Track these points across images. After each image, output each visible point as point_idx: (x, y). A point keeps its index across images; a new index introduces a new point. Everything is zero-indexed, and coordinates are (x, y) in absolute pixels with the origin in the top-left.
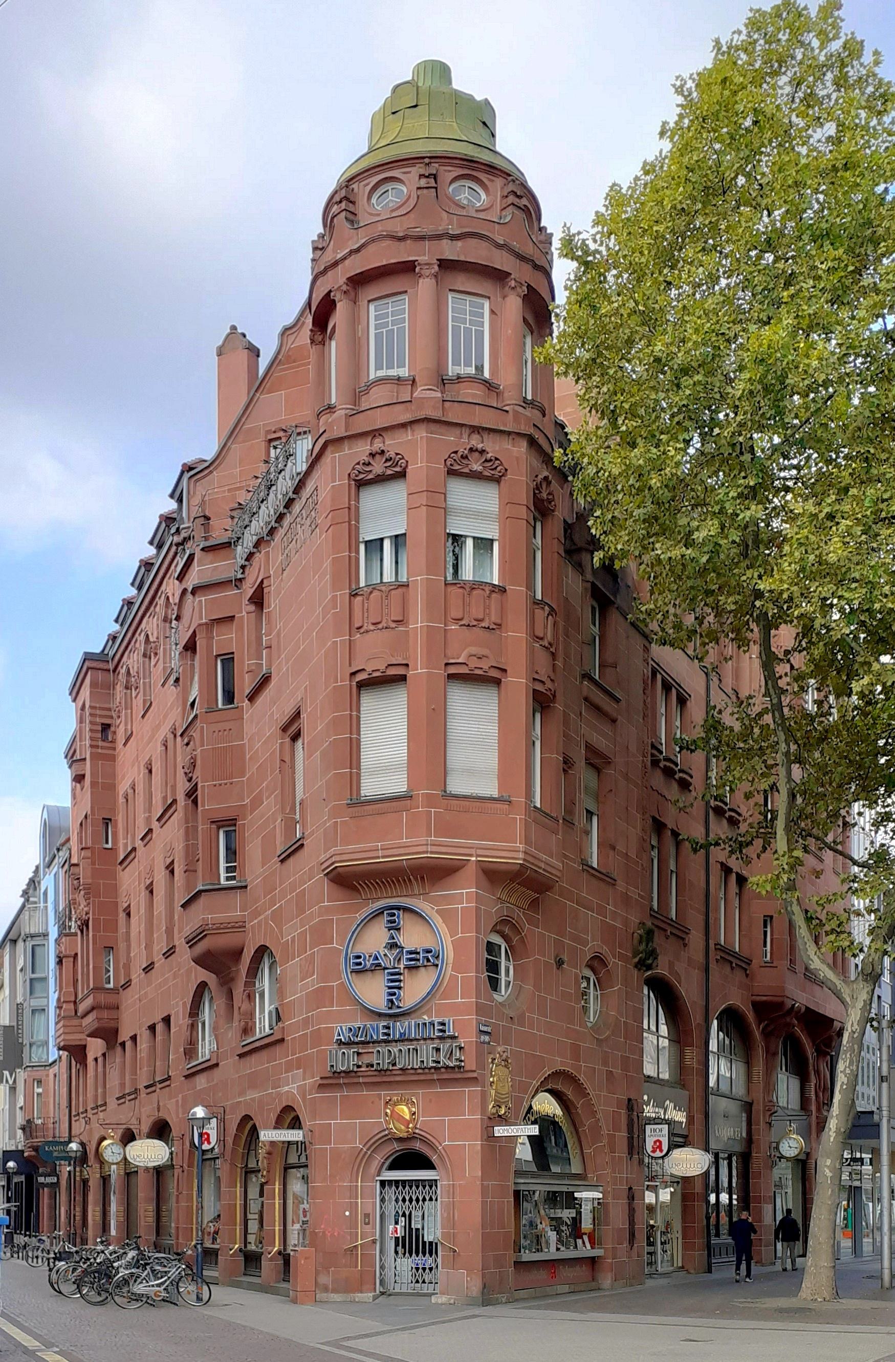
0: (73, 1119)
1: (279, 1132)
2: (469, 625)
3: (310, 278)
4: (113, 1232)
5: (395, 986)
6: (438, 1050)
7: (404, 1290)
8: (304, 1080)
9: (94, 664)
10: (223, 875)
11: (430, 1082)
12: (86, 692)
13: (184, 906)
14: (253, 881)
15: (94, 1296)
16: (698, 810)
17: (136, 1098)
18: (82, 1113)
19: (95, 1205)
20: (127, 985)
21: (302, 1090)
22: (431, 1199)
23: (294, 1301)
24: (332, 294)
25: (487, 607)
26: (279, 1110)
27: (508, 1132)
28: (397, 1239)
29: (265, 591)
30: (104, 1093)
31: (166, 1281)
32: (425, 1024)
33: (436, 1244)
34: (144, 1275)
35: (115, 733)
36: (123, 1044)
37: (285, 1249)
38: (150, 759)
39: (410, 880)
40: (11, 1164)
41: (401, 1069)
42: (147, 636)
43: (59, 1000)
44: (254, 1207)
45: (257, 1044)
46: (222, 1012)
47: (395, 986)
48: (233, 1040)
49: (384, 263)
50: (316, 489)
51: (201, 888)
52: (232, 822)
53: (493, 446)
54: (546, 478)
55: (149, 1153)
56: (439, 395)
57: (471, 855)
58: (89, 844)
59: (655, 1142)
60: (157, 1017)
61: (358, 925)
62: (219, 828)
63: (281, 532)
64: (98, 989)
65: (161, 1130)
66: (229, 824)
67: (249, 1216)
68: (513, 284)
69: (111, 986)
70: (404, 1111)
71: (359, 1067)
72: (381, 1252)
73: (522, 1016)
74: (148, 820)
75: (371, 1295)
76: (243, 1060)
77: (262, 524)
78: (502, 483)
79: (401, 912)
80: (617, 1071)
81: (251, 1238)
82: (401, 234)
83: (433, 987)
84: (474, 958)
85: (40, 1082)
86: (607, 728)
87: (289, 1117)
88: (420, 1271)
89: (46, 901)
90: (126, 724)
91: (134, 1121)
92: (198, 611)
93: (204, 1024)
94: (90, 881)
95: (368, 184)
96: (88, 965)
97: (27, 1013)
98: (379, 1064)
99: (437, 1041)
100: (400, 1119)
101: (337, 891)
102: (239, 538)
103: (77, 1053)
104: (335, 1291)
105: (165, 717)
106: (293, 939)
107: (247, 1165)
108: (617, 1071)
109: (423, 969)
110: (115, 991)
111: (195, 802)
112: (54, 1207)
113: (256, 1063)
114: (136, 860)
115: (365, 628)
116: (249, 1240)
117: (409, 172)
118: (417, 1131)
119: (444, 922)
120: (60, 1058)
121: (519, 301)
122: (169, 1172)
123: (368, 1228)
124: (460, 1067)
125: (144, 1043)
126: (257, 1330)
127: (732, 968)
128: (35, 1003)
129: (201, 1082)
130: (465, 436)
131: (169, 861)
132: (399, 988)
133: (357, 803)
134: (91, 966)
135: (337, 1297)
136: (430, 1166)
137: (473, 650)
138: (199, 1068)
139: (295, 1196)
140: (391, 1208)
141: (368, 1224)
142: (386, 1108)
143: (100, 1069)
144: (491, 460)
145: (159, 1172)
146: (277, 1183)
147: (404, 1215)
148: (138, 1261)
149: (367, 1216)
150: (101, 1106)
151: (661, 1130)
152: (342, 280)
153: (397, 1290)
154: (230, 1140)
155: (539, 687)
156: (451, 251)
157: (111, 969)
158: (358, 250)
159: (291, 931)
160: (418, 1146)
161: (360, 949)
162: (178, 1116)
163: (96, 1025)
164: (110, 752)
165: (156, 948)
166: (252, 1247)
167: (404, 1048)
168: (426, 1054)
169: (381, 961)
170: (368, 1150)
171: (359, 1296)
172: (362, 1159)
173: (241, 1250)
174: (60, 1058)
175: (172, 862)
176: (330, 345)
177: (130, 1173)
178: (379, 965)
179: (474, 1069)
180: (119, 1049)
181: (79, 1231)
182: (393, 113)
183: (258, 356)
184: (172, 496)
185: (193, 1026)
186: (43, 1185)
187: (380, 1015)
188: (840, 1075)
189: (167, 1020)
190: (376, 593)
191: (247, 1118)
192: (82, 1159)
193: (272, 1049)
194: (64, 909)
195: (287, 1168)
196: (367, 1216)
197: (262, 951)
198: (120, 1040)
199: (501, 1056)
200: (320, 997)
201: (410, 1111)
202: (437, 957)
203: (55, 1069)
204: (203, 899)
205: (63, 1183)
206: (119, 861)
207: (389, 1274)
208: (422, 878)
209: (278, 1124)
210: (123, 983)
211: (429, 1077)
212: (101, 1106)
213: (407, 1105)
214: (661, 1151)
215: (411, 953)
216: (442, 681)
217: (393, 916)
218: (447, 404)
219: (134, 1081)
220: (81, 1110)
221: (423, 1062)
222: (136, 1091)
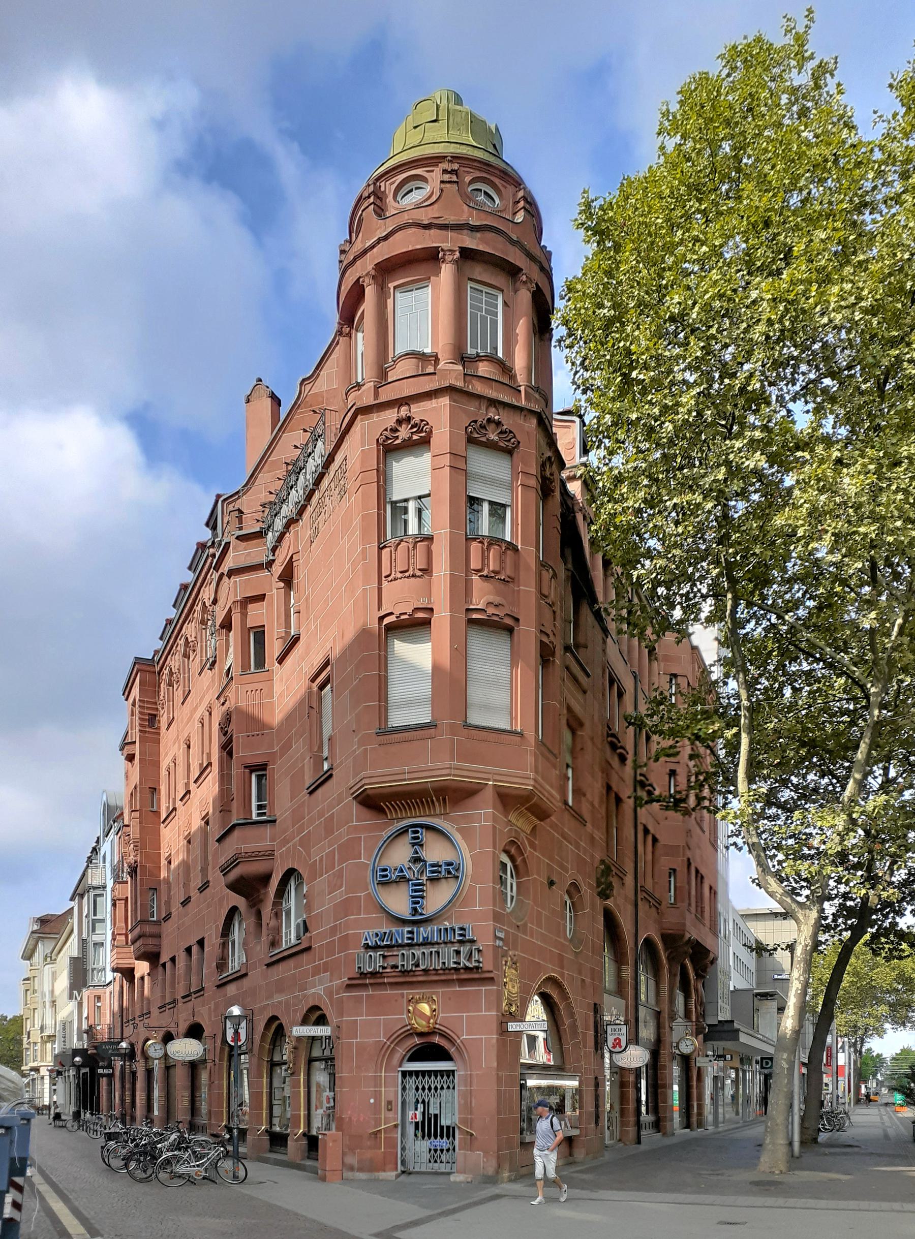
2: (487, 576)
3: (339, 275)
4: (156, 1113)
5: (418, 897)
6: (458, 953)
7: (423, 1169)
8: (331, 981)
9: (144, 667)
12: (136, 692)
13: (219, 841)
14: (282, 815)
15: (139, 1174)
16: (630, 782)
20: (168, 917)
21: (329, 992)
22: (448, 1087)
23: (323, 1179)
24: (361, 280)
25: (502, 562)
28: (417, 1124)
29: (295, 564)
31: (206, 1162)
32: (446, 929)
33: (454, 1128)
34: (185, 1157)
35: (159, 721)
36: (164, 965)
37: (309, 1131)
38: (189, 736)
39: (432, 801)
40: (77, 1059)
41: (423, 970)
42: (187, 638)
43: (113, 933)
45: (285, 954)
46: (252, 928)
47: (418, 897)
48: (262, 951)
49: (410, 249)
50: (345, 459)
51: (236, 822)
52: (263, 767)
53: (508, 420)
54: (549, 458)
55: (186, 1049)
56: (461, 368)
57: (489, 780)
58: (138, 808)
59: (615, 1040)
60: (193, 941)
62: (251, 772)
63: (309, 509)
64: (143, 921)
65: (195, 1032)
66: (260, 769)
67: (275, 1102)
68: (524, 278)
69: (155, 919)
70: (425, 1008)
71: (384, 968)
72: (402, 1135)
73: (525, 925)
74: (187, 784)
75: (394, 1173)
76: (270, 969)
77: (291, 507)
78: (515, 455)
79: (424, 830)
80: (588, 980)
81: (276, 1121)
82: (426, 222)
83: (454, 896)
84: (489, 871)
86: (580, 696)
88: (438, 1152)
89: (104, 862)
90: (169, 713)
91: (173, 1025)
92: (233, 590)
95: (393, 183)
97: (91, 945)
98: (403, 965)
99: (457, 945)
100: (422, 1015)
101: (365, 812)
102: (269, 527)
104: (360, 1170)
105: (202, 699)
106: (321, 859)
107: (272, 1059)
108: (588, 980)
109: (443, 881)
110: (158, 923)
111: (230, 754)
112: (110, 1092)
115: (393, 576)
116: (274, 1122)
117: (432, 171)
118: (437, 1026)
119: (463, 838)
121: (529, 295)
122: (202, 1066)
123: (391, 1115)
124: (477, 968)
125: (181, 962)
126: (302, 1216)
127: (650, 907)
128: (96, 938)
129: (231, 989)
130: (484, 408)
131: (204, 814)
132: (422, 897)
133: (385, 732)
136: (447, 1057)
137: (491, 598)
138: (230, 978)
139: (318, 1085)
140: (411, 1095)
141: (391, 1110)
142: (408, 1005)
144: (506, 432)
145: (194, 1067)
147: (423, 1102)
148: (179, 1143)
149: (389, 1103)
150: (147, 1014)
151: (620, 1030)
152: (370, 267)
153: (416, 1170)
154: (257, 1037)
155: (545, 640)
156: (470, 242)
158: (386, 238)
159: (319, 852)
160: (437, 1039)
161: (385, 863)
162: (210, 1019)
164: (156, 736)
166: (277, 1128)
167: (426, 951)
168: (448, 957)
171: (382, 1175)
172: (384, 1052)
173: (267, 1131)
176: (356, 335)
177: (169, 1067)
178: (404, 877)
179: (491, 969)
180: (160, 969)
181: (129, 1111)
182: (415, 127)
183: (280, 405)
184: (207, 525)
185: (224, 945)
186: (103, 1075)
187: (404, 922)
188: (795, 982)
189: (201, 943)
190: (403, 544)
191: (274, 1018)
192: (130, 1055)
193: (299, 957)
194: (119, 861)
195: (311, 1061)
196: (389, 1103)
197: (290, 873)
198: (162, 961)
199: (512, 959)
200: (346, 907)
202: (457, 870)
204: (236, 833)
205: (117, 1073)
207: (409, 1154)
208: (444, 800)
209: (305, 1022)
210: (164, 916)
211: (449, 977)
212: (147, 1014)
213: (427, 1003)
214: (620, 1047)
215: (433, 866)
216: (463, 624)
217: (416, 834)
218: (468, 378)
219: (173, 993)
221: (444, 963)
222: (174, 1001)
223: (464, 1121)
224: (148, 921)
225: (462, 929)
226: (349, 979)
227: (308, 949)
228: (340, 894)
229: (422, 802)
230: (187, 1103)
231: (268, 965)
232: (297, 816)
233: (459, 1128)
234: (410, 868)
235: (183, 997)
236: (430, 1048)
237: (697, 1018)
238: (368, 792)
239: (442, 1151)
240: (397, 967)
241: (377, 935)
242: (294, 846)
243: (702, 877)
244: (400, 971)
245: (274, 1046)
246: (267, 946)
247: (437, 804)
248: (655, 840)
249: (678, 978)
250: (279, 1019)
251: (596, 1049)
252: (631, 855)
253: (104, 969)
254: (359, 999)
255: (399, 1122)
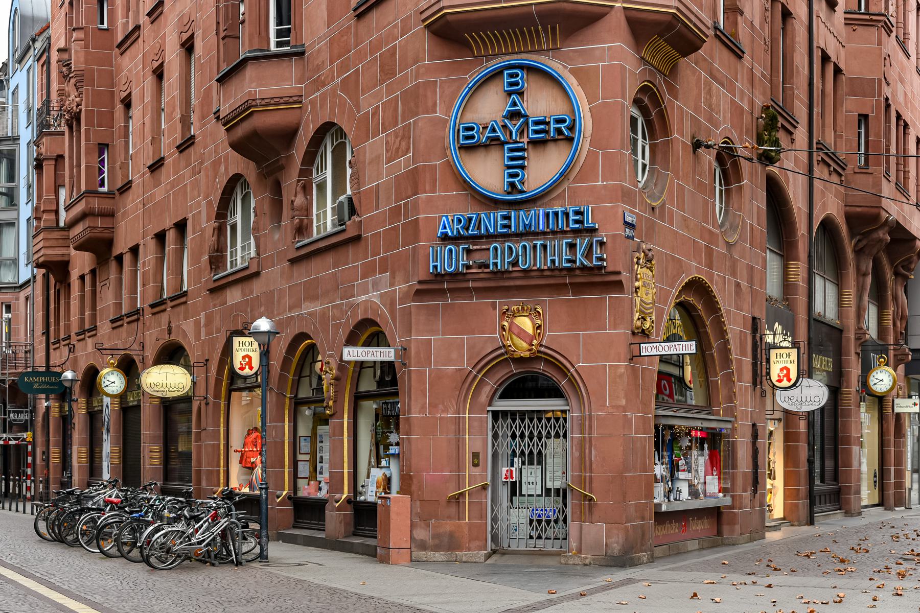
0: (52, 347)
1: (371, 349)
5: (516, 166)
6: (572, 246)
7: (522, 547)
8: (392, 285)
10: (273, 39)
11: (558, 288)
17: (138, 320)
18: (64, 340)
19: (81, 445)
20: (127, 187)
23: (385, 560)
26: (352, 324)
27: (658, 349)
30: (94, 317)
32: (556, 214)
36: (119, 259)
39: (537, 31)
41: (524, 271)
44: (305, 446)
47: (516, 166)
48: (282, 240)
58: (83, 23)
61: (470, 89)
65: (171, 354)
67: (300, 457)
69: (105, 189)
70: (526, 323)
71: (468, 267)
73: (663, 206)
75: (483, 553)
80: (744, 284)
83: (568, 166)
85: (9, 308)
87: (368, 331)
91: (135, 347)
93: (234, 228)
94: (82, 67)
96: (79, 166)
100: (521, 333)
103: (56, 270)
104: (436, 548)
107: (296, 396)
110: (110, 195)
113: (322, 270)
114: (140, 40)
118: (542, 349)
120: (34, 277)
123: (477, 471)
124: (600, 268)
125: (148, 255)
131: (185, 36)
132: (522, 167)
134: (83, 167)
135: (439, 556)
136: (555, 392)
143: (88, 287)
146: (346, 416)
147: (523, 453)
149: (475, 455)
150: (90, 330)
151: (789, 355)
153: (514, 547)
157: (106, 170)
160: (541, 367)
163: (88, 234)
165: (165, 141)
168: (558, 253)
169: (499, 134)
170: (479, 372)
172: (467, 384)
173: (290, 498)
174: (34, 277)
175: (192, 37)
178: (498, 138)
180: (113, 265)
187: (493, 203)
189: (181, 227)
197: (326, 129)
198: (116, 251)
199: (646, 255)
200: (412, 181)
201: (534, 324)
202: (571, 128)
203: (28, 291)
204: (250, 71)
206: (116, 44)
207: (502, 525)
208: (554, 29)
209: (351, 341)
210: (119, 185)
212: (90, 330)
214: (789, 380)
215: (537, 123)
220: (62, 336)
221: (553, 261)
223: (581, 481)
224: (97, 193)
225: (577, 213)
226: (420, 282)
227: (357, 239)
228: (404, 163)
229: (522, 33)
230: (156, 462)
231: (293, 261)
232: (338, 48)
233: (572, 490)
234: (505, 126)
235: (152, 306)
236: (532, 379)
237: (896, 339)
238: (449, 18)
239: (548, 522)
240: (487, 266)
241: (459, 221)
242: (334, 91)
243: (906, 125)
244: (492, 272)
245: (300, 377)
246: (290, 233)
247: (542, 35)
248: (838, 71)
249: (869, 280)
250: (309, 338)
251: (755, 384)
252: (804, 97)
253: (15, 262)
254: (434, 311)
255: (489, 482)
